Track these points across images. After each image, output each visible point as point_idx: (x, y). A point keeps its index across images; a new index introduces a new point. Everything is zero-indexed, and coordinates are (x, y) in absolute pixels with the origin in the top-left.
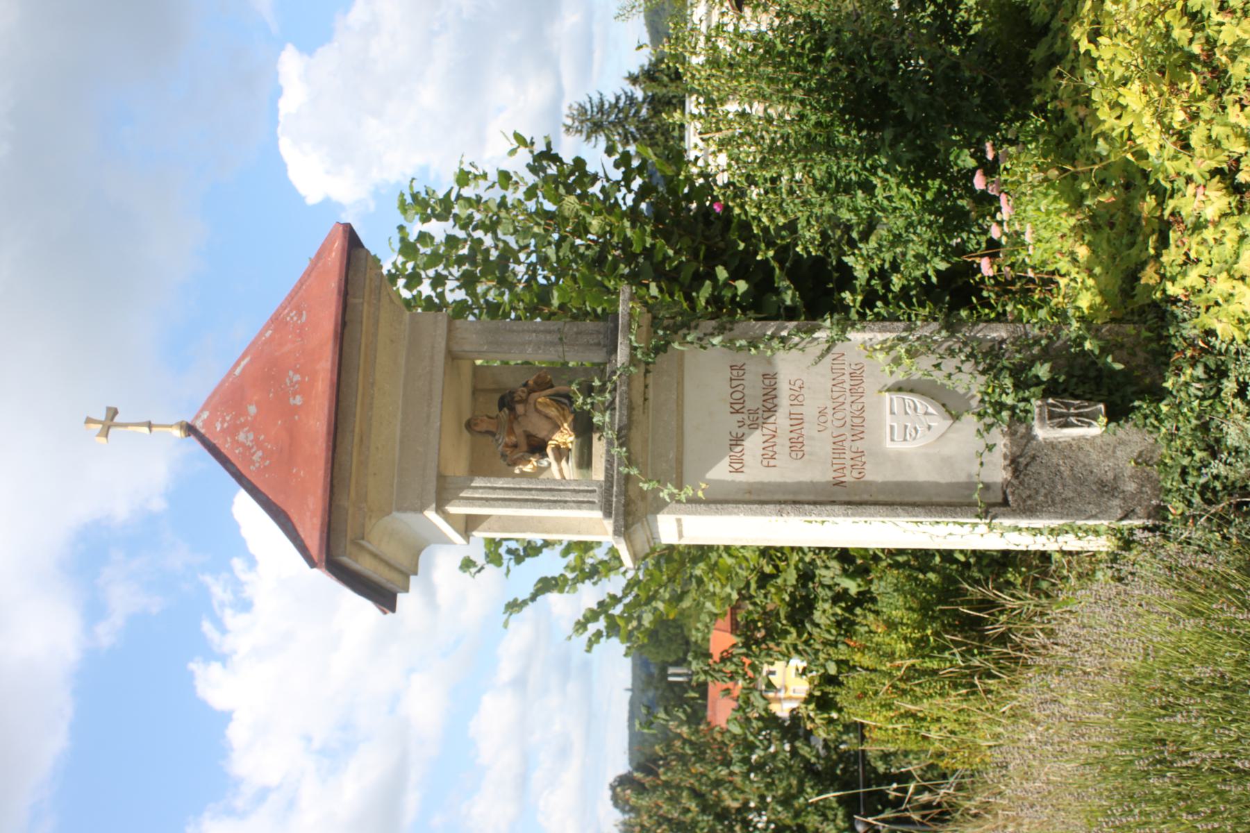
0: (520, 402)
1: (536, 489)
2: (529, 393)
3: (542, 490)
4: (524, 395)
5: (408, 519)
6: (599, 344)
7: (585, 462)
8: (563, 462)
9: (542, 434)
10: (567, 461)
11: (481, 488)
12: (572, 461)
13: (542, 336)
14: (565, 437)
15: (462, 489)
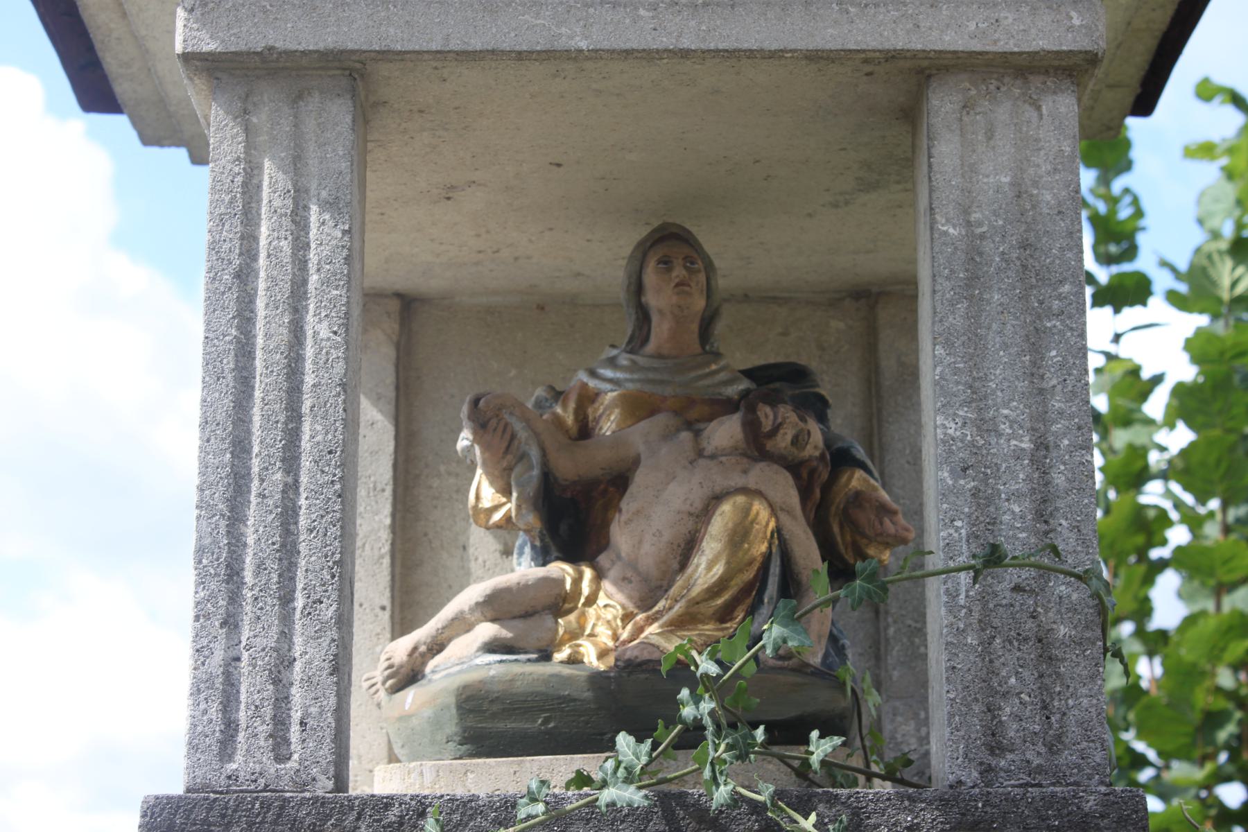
0: (752, 428)
1: (291, 489)
2: (794, 468)
3: (288, 514)
4: (783, 441)
5: (1154, 692)
6: (996, 746)
7: (489, 725)
8: (487, 630)
9: (622, 536)
10: (492, 647)
11: (300, 246)
12: (492, 667)
13: (1020, 478)
14: (604, 626)
15: (296, 165)
